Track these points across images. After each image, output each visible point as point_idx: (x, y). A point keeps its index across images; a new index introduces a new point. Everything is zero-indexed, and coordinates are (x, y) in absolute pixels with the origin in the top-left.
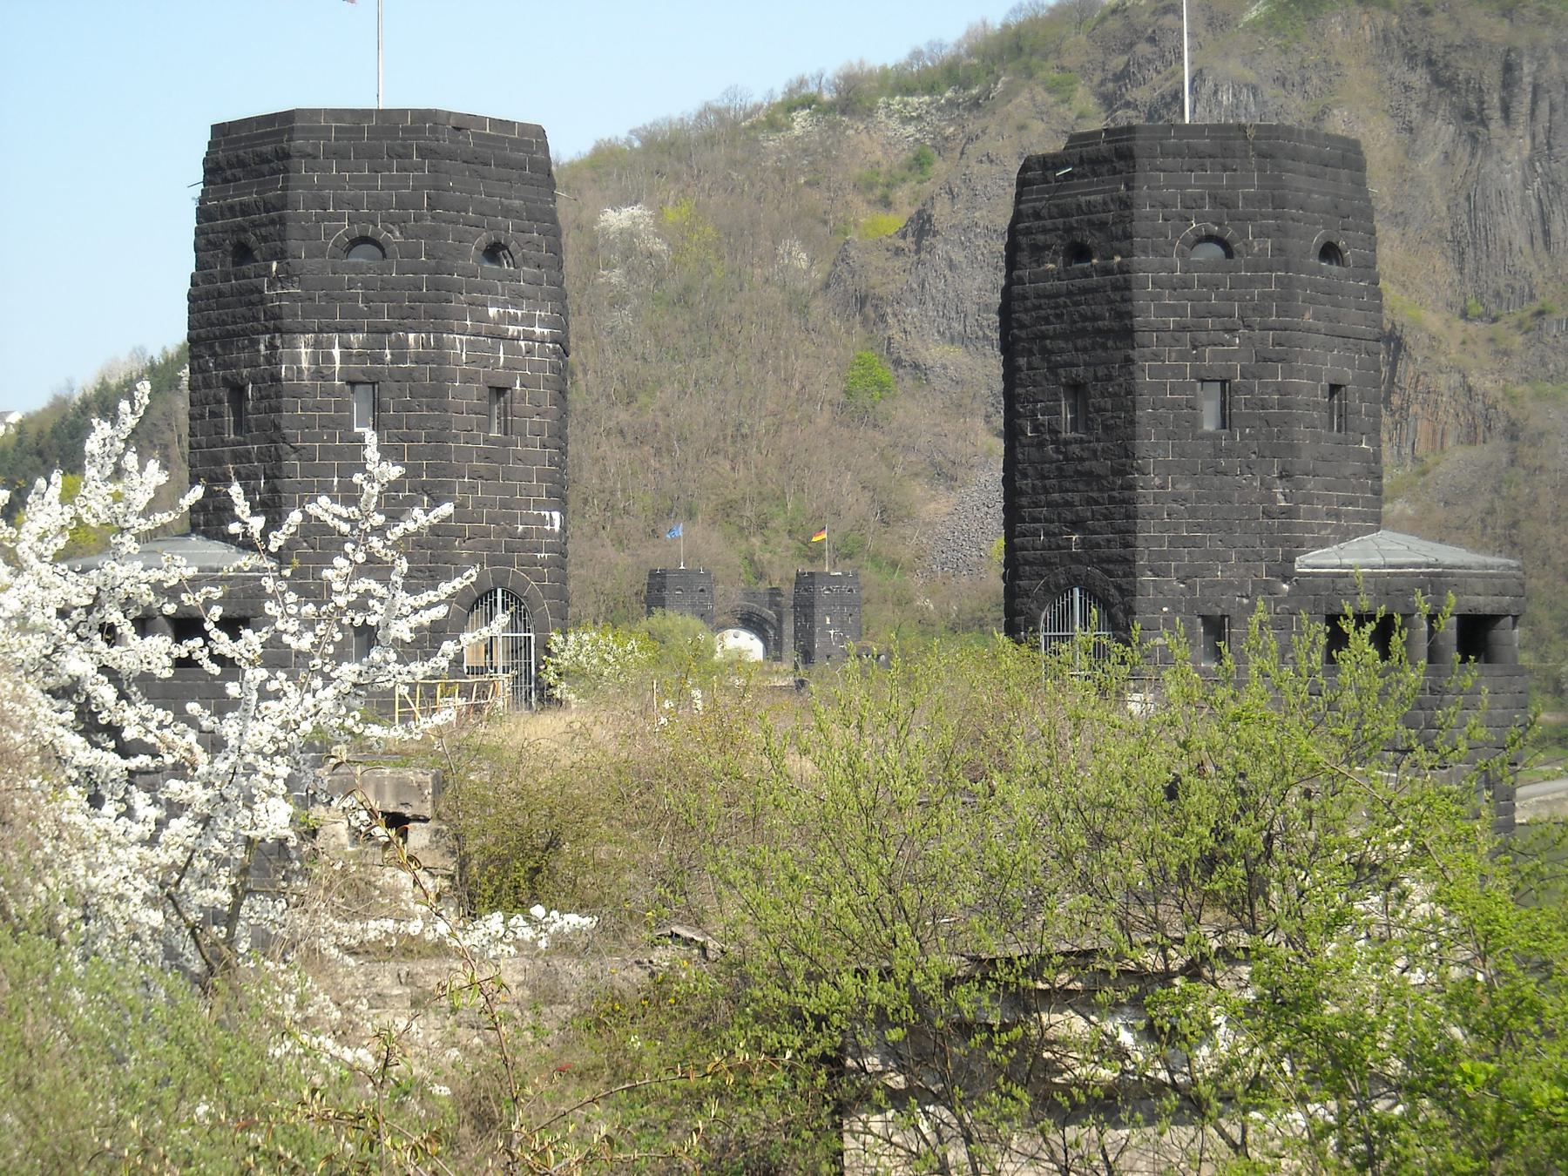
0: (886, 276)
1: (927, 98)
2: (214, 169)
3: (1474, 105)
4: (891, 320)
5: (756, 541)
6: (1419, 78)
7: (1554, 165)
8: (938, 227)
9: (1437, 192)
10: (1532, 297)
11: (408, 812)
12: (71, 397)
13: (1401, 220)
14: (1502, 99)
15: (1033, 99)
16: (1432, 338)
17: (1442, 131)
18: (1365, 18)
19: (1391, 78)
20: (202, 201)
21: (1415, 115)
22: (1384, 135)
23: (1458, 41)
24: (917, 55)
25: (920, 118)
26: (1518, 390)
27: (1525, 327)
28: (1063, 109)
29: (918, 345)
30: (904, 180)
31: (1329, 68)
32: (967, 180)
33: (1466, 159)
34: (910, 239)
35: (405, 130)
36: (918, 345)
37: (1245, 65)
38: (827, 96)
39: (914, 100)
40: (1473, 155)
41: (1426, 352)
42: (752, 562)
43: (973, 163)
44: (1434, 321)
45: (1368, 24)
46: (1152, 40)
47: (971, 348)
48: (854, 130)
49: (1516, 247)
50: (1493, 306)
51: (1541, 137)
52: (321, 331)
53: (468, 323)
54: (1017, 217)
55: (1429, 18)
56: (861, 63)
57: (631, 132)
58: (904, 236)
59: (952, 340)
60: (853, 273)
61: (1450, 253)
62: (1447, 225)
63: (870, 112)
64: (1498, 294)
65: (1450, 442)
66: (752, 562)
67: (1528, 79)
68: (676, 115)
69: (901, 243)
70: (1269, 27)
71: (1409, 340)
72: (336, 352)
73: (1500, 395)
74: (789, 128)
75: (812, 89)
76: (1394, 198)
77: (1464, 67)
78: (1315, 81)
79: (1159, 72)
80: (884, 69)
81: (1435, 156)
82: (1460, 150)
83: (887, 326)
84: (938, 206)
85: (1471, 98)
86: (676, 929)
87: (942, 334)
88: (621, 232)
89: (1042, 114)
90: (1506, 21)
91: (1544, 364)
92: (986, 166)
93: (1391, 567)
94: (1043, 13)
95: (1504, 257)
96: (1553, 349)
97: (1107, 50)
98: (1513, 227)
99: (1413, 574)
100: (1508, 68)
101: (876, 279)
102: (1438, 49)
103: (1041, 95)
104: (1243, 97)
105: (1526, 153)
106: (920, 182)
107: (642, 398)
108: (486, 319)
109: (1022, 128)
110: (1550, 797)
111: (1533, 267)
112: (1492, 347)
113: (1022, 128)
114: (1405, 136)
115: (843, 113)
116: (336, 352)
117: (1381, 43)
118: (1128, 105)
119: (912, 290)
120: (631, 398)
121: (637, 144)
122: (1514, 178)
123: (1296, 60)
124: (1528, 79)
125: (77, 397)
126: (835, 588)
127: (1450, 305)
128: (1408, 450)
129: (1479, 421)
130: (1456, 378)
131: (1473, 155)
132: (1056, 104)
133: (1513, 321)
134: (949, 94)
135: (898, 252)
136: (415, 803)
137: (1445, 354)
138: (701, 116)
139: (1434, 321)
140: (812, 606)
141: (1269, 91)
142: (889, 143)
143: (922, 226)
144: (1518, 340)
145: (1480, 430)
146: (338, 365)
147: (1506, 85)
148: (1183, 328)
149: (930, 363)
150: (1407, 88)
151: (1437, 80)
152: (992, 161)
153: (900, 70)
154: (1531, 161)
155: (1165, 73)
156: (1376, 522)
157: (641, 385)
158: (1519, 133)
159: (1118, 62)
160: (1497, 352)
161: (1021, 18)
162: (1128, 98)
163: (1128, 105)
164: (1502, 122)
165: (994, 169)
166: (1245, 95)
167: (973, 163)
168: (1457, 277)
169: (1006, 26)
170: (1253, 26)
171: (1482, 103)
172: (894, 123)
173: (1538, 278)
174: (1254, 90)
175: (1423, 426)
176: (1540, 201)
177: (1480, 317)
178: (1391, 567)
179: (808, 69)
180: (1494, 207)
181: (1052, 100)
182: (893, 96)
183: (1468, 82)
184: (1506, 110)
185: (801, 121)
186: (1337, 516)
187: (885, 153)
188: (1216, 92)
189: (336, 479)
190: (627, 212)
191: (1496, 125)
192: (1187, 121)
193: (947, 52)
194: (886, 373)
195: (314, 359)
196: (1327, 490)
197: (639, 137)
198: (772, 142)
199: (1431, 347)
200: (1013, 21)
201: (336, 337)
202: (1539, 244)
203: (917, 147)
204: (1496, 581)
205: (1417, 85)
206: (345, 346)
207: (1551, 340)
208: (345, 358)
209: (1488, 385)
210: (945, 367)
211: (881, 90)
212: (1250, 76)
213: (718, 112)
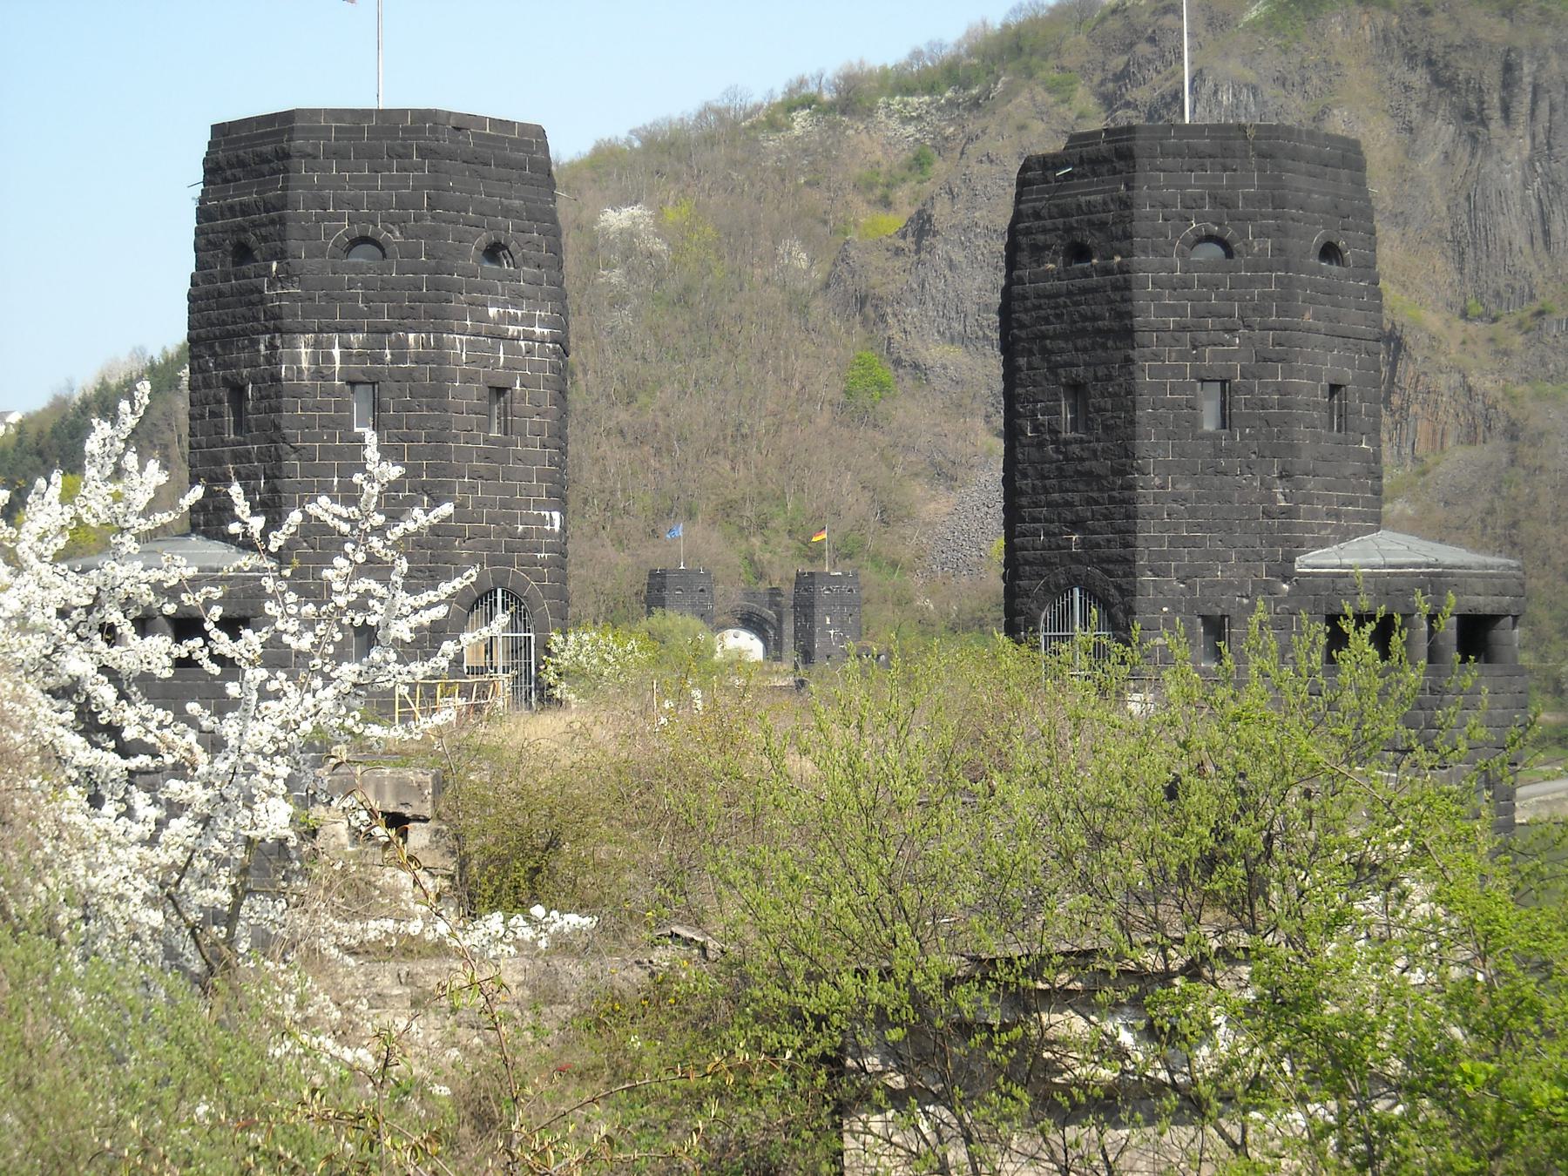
0: (886, 276)
1: (927, 98)
2: (214, 169)
3: (1474, 105)
4: (891, 320)
5: (756, 541)
6: (1419, 78)
7: (1554, 165)
8: (938, 227)
9: (1437, 192)
10: (1532, 297)
11: (408, 812)
12: (71, 397)
13: (1401, 220)
14: (1502, 99)
15: (1033, 99)
16: (1432, 338)
17: (1442, 131)
18: (1365, 18)
19: (1391, 78)
20: (202, 201)
21: (1415, 115)
22: (1384, 135)
23: (1458, 41)
24: (917, 55)
25: (920, 118)
26: (1518, 390)
27: (1525, 327)
28: (1063, 109)
29: (918, 345)
30: (904, 180)
31: (1329, 68)
32: (967, 180)
33: (1466, 159)
34: (910, 239)
35: (405, 130)
36: (918, 345)
37: (1245, 65)
38: (827, 96)
39: (914, 100)
40: (1473, 155)
41: (1426, 352)
42: (752, 562)
43: (973, 163)
44: (1434, 321)
45: (1368, 24)
46: (1152, 40)
47: (971, 348)
48: (854, 130)
49: (1516, 247)
50: (1493, 306)
51: (1541, 137)
52: (321, 331)
53: (468, 323)
54: (1017, 217)
55: (1429, 18)
56: (861, 63)
57: (631, 132)
58: (904, 236)
59: (952, 340)
60: (853, 273)
61: (1450, 253)
62: (1447, 225)
63: (870, 112)
64: (1498, 294)
65: (1450, 442)
66: (752, 562)
67: (1528, 79)
68: (676, 115)
69: (901, 243)
70: (1269, 27)
71: (1409, 340)
72: (336, 352)
73: (1500, 395)
74: (789, 128)
75: (812, 89)
76: (1394, 198)
77: (1464, 67)
78: (1315, 81)
79: (1159, 72)
80: (884, 69)
81: (1435, 156)
82: (1460, 150)
83: (887, 326)
84: (938, 206)
85: (1471, 98)
86: (676, 929)
87: (942, 334)
88: (621, 232)
89: (1042, 114)
90: (1506, 21)
91: (1544, 364)
92: (986, 166)
93: (1391, 567)
94: (1043, 13)
95: (1504, 257)
96: (1553, 349)
97: (1107, 50)
98: (1513, 227)
99: (1413, 574)
100: (1508, 68)
101: (876, 279)
102: (1438, 49)
103: (1041, 95)
104: (1243, 97)
105: (1526, 153)
106: (920, 182)
107: (642, 398)
108: (486, 319)
109: (1022, 128)
110: (1550, 797)
111: (1533, 267)
112: (1492, 347)
113: (1022, 128)
114: (1405, 136)
115: (843, 113)
116: (336, 352)
117: (1381, 43)
118: (1128, 105)
119: (912, 290)
120: (631, 398)
121: (637, 144)
122: (1514, 178)
123: (1296, 60)
124: (1528, 79)
125: (77, 397)
126: (835, 588)
127: (1450, 305)
128: (1408, 450)
129: (1479, 421)
130: (1456, 378)
131: (1473, 155)
132: (1056, 104)
133: (1513, 321)
134: (949, 94)
135: (898, 252)
136: (415, 803)
137: (1445, 354)
138: (701, 116)
139: (1434, 321)
140: (812, 606)
141: (1269, 91)
142: (889, 143)
143: (922, 226)
144: (1518, 340)
145: (1480, 430)
146: (338, 365)
147: (1506, 85)
148: (1183, 328)
149: (930, 363)
150: (1407, 88)
151: (1437, 80)
152: (992, 161)
153: (900, 70)
154: (1531, 161)
155: (1165, 73)
156: (1376, 522)
157: (641, 385)
158: (1519, 133)
159: (1118, 62)
160: (1497, 352)
161: (1021, 18)
162: (1128, 98)
163: (1128, 105)
164: (1502, 122)
165: (994, 169)
166: (1245, 95)
167: (973, 163)
168: (1457, 277)
169: (1006, 26)
170: (1253, 26)
171: (1482, 103)
172: (894, 123)
173: (1538, 278)
174: (1254, 90)
175: (1423, 426)
176: (1540, 201)
177: (1480, 317)
178: (1391, 567)
179: (808, 69)
180: (1494, 207)
181: (1052, 100)
182: (893, 96)
183: (1468, 82)
184: (1506, 110)
185: (801, 121)
186: (1337, 516)
187: (885, 153)
188: (1216, 92)
189: (336, 479)
190: (627, 212)
191: (1496, 125)
192: (1187, 121)
193: (947, 52)
194: (886, 373)
195: (314, 359)
196: (1327, 490)
197: (639, 137)
198: (772, 142)
199: (1431, 347)
200: (1013, 21)
201: (336, 337)
202: (1539, 244)
203: (917, 147)
204: (1496, 581)
205: (1417, 85)
206: (345, 346)
207: (1551, 340)
208: (345, 358)
209: (1488, 385)
210: (945, 367)
211: (881, 90)
212: (1250, 76)
213: (718, 112)
